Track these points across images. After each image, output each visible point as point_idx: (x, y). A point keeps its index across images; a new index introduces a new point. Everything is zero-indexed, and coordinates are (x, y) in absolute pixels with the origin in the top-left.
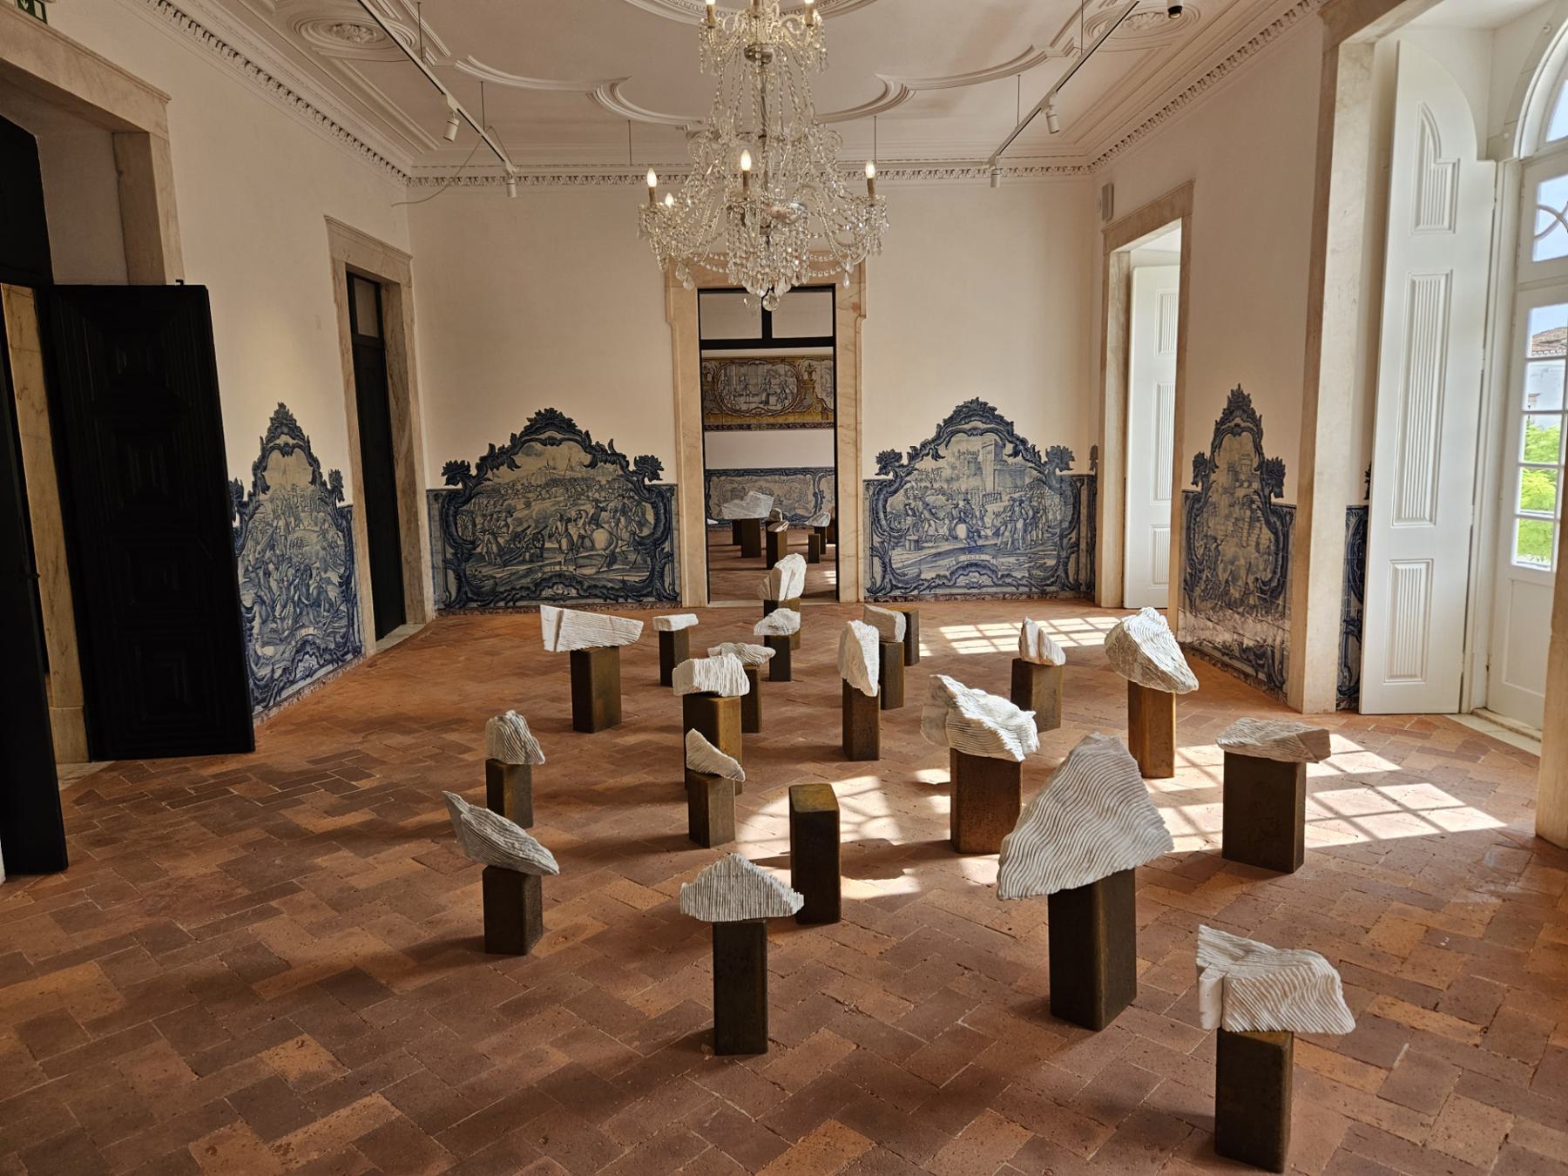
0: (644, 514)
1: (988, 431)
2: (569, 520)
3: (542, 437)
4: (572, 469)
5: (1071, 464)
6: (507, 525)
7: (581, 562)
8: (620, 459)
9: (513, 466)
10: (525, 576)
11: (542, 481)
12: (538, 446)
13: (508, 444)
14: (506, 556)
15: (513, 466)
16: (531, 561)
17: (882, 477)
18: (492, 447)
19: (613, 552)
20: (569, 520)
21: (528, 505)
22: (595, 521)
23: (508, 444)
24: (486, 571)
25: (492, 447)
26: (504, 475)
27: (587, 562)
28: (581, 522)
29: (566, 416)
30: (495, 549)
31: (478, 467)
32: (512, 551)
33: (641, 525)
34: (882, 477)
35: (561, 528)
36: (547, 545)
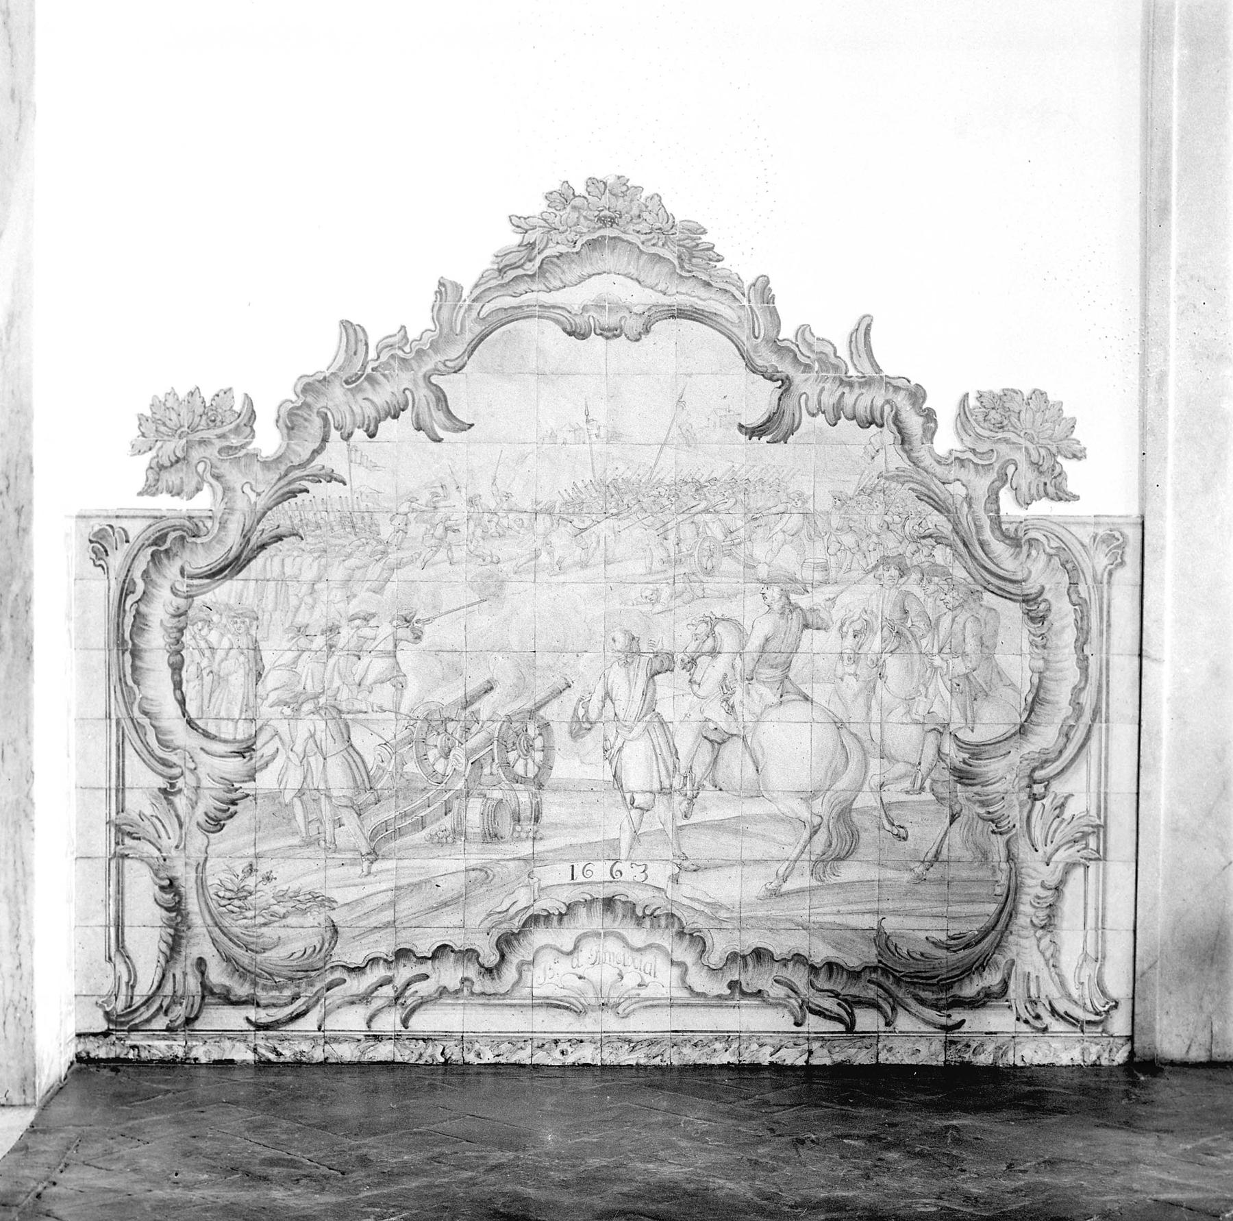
0: (986, 647)
1: (310, 460)
2: (663, 664)
3: (574, 298)
4: (690, 441)
5: (1075, 474)
6: (397, 680)
7: (699, 846)
8: (895, 414)
9: (440, 418)
10: (460, 900)
11: (555, 487)
12: (551, 336)
13: (420, 323)
14: (384, 818)
15: (440, 418)
16: (492, 836)
17: (164, 503)
18: (351, 332)
19: (845, 813)
20: (663, 664)
21: (491, 590)
22: (777, 667)
23: (420, 323)
24: (296, 873)
25: (351, 332)
26: (384, 468)
27: (729, 846)
28: (712, 672)
29: (681, 209)
30: (338, 778)
31: (291, 422)
32: (406, 789)
33: (973, 691)
34: (164, 503)
35: (628, 697)
36: (564, 768)
